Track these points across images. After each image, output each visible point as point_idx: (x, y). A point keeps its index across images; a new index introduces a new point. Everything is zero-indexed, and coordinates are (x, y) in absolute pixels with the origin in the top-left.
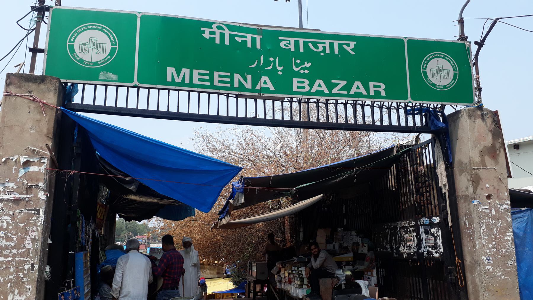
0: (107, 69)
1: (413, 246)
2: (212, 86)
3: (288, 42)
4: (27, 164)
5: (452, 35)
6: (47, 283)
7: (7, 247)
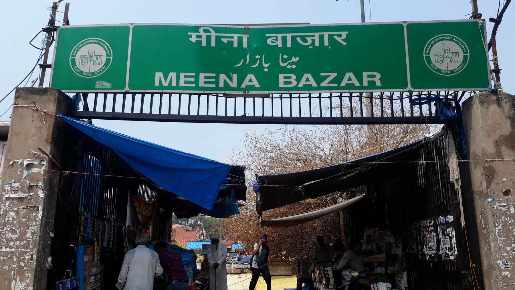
0: (102, 78)
1: (434, 248)
2: (198, 88)
3: (275, 38)
4: (30, 166)
5: (462, 13)
6: (49, 272)
7: (12, 240)
